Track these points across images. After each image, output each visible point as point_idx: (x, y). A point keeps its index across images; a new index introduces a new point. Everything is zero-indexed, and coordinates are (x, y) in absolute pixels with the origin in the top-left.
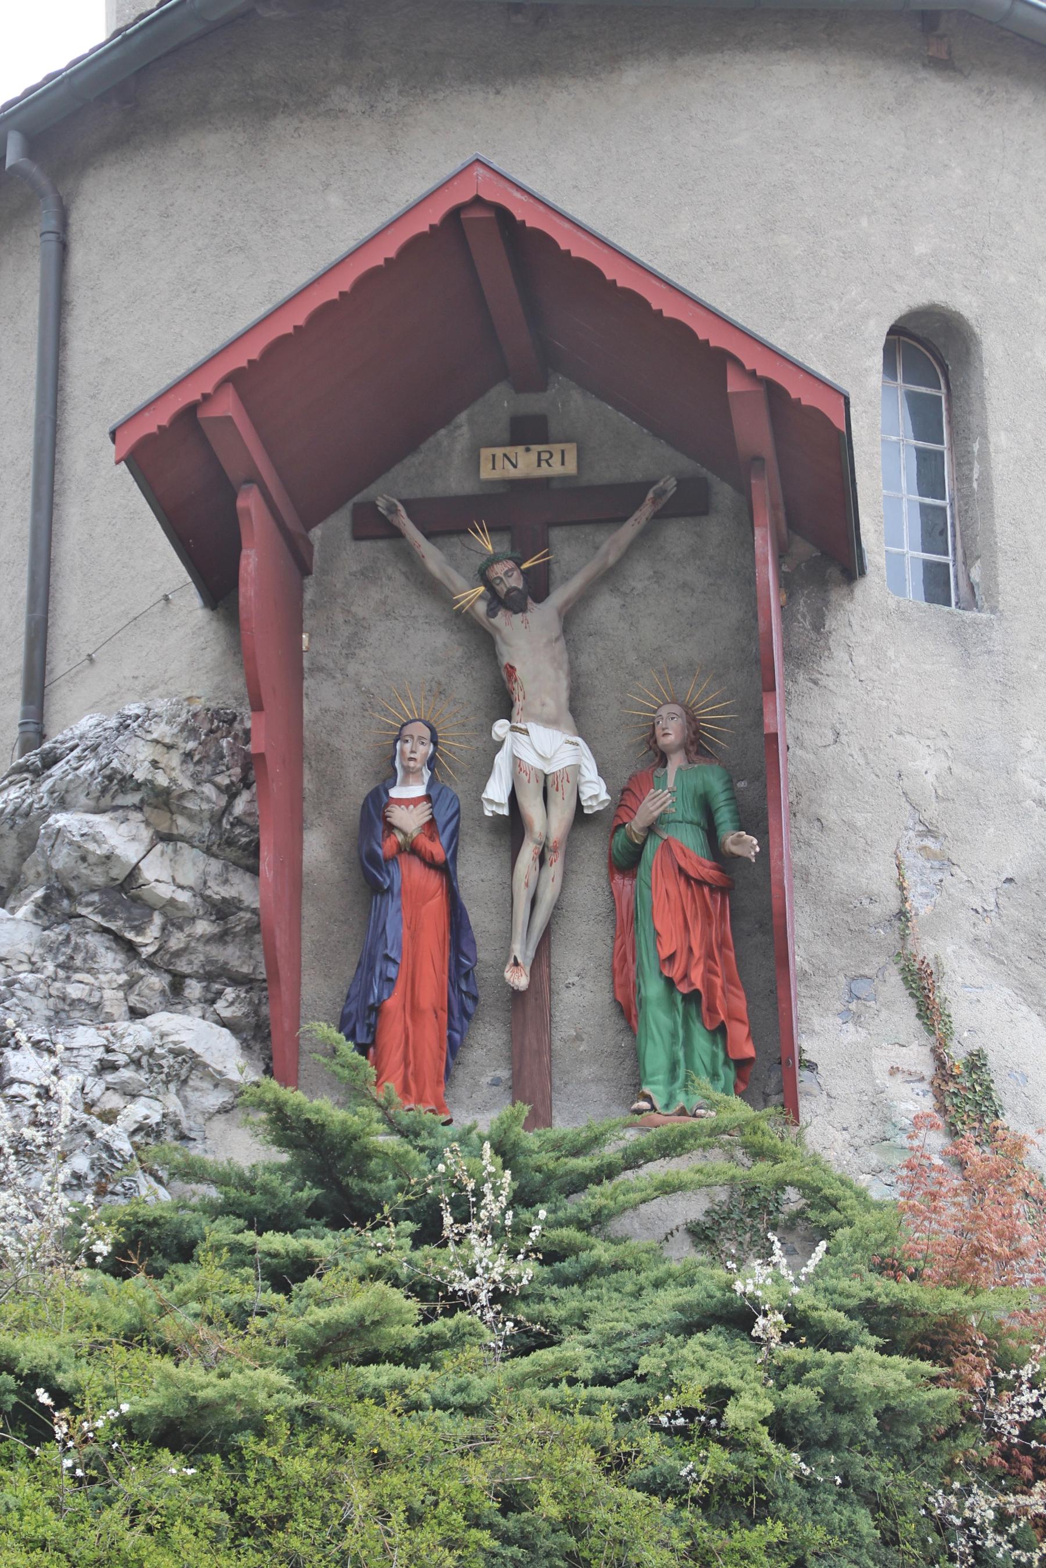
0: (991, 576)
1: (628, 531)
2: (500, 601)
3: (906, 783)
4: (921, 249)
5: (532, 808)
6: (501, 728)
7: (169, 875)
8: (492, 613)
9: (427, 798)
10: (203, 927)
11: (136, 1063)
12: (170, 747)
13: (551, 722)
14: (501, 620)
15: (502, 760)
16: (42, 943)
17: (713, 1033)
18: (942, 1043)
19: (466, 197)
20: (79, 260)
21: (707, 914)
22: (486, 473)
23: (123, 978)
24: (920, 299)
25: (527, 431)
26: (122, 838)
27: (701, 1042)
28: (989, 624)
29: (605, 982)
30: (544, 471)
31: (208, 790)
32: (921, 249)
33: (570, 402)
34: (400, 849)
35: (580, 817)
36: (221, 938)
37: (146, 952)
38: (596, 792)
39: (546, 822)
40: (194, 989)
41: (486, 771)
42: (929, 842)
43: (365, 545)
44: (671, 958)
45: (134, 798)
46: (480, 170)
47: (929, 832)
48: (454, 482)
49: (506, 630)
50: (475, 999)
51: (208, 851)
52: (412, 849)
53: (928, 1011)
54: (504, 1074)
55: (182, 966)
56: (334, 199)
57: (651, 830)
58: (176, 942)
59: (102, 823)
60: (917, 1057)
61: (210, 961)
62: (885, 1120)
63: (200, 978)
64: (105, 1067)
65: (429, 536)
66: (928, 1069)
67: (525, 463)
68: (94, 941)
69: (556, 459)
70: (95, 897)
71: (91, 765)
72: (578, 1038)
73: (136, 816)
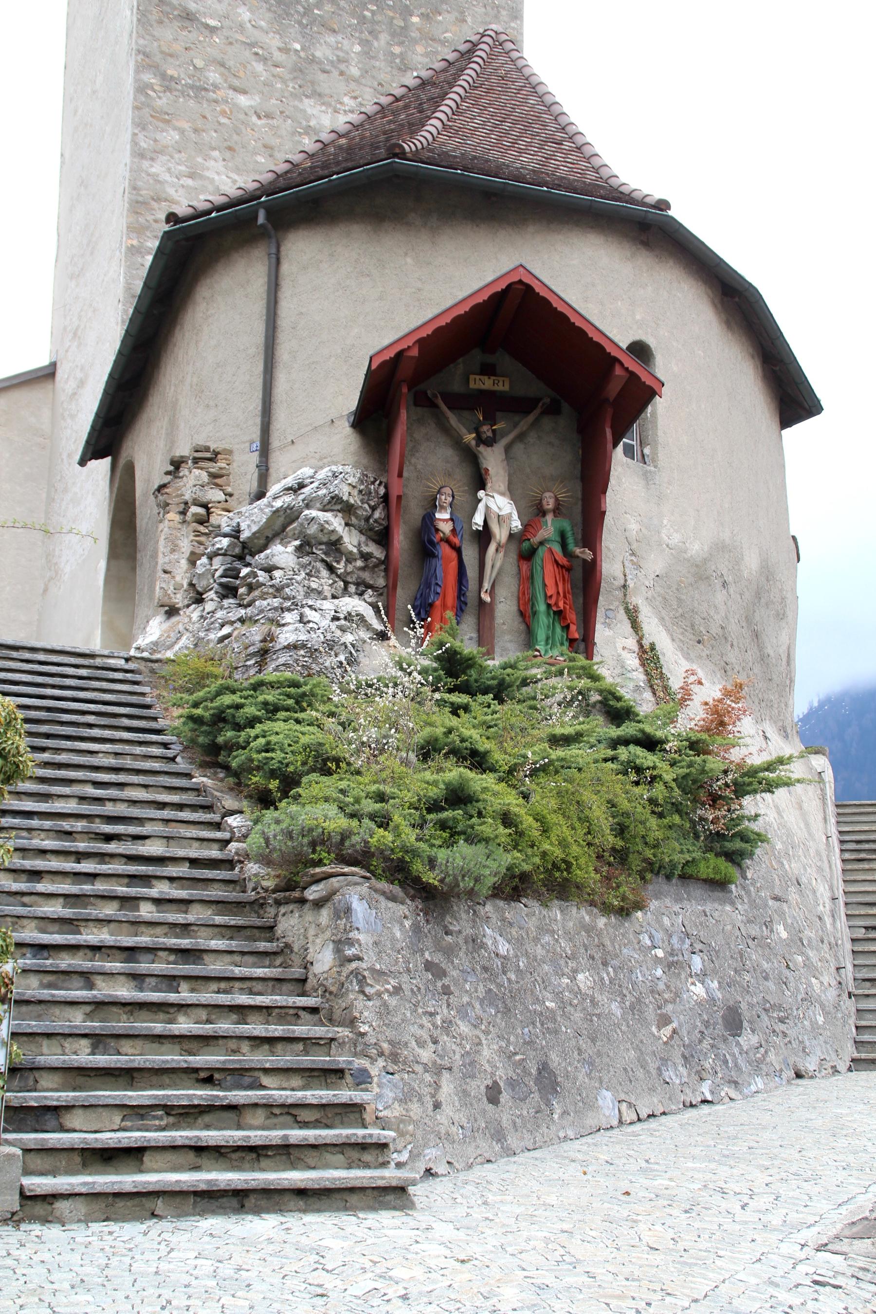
0: (655, 452)
1: (531, 418)
2: (481, 440)
3: (627, 534)
4: (638, 317)
5: (494, 527)
6: (481, 494)
7: (351, 541)
8: (478, 445)
9: (452, 519)
10: (359, 563)
11: (345, 618)
12: (354, 487)
13: (502, 494)
14: (482, 448)
15: (481, 506)
16: (299, 564)
17: (563, 628)
18: (641, 638)
19: (516, 280)
20: (285, 268)
21: (564, 580)
22: (472, 385)
23: (331, 582)
24: (637, 338)
25: (488, 370)
26: (336, 522)
27: (558, 630)
28: (655, 472)
29: (515, 602)
30: (496, 388)
31: (366, 506)
32: (638, 317)
33: (504, 360)
34: (442, 540)
35: (511, 536)
36: (363, 569)
37: (339, 572)
38: (516, 524)
39: (500, 534)
40: (352, 588)
41: (474, 509)
42: (633, 558)
43: (419, 409)
44: (551, 597)
45: (338, 507)
46: (521, 269)
47: (633, 554)
48: (457, 387)
49: (485, 453)
50: (466, 604)
51: (361, 532)
52: (447, 541)
53: (635, 625)
54: (474, 635)
55: (349, 579)
56: (409, 260)
57: (541, 543)
58: (350, 568)
59: (328, 516)
60: (631, 643)
61: (359, 577)
62: (623, 667)
63: (354, 584)
64: (335, 619)
65: (449, 408)
66: (636, 648)
67: (487, 383)
68: (319, 565)
69: (501, 384)
70: (323, 547)
71: (323, 491)
72: (504, 624)
73: (340, 515)
